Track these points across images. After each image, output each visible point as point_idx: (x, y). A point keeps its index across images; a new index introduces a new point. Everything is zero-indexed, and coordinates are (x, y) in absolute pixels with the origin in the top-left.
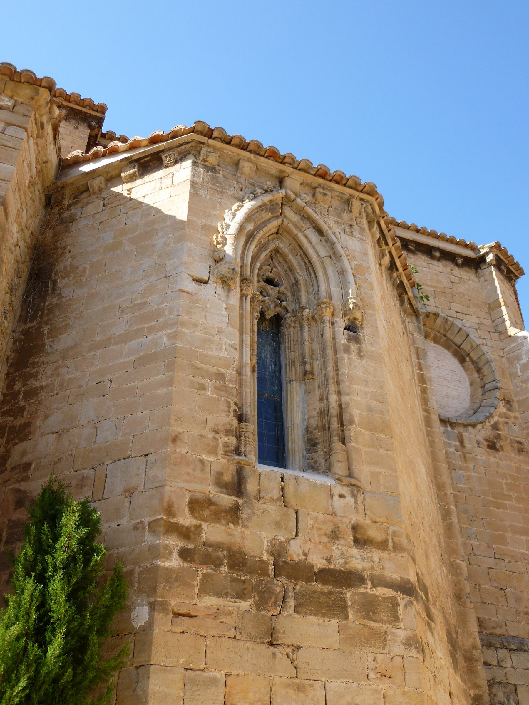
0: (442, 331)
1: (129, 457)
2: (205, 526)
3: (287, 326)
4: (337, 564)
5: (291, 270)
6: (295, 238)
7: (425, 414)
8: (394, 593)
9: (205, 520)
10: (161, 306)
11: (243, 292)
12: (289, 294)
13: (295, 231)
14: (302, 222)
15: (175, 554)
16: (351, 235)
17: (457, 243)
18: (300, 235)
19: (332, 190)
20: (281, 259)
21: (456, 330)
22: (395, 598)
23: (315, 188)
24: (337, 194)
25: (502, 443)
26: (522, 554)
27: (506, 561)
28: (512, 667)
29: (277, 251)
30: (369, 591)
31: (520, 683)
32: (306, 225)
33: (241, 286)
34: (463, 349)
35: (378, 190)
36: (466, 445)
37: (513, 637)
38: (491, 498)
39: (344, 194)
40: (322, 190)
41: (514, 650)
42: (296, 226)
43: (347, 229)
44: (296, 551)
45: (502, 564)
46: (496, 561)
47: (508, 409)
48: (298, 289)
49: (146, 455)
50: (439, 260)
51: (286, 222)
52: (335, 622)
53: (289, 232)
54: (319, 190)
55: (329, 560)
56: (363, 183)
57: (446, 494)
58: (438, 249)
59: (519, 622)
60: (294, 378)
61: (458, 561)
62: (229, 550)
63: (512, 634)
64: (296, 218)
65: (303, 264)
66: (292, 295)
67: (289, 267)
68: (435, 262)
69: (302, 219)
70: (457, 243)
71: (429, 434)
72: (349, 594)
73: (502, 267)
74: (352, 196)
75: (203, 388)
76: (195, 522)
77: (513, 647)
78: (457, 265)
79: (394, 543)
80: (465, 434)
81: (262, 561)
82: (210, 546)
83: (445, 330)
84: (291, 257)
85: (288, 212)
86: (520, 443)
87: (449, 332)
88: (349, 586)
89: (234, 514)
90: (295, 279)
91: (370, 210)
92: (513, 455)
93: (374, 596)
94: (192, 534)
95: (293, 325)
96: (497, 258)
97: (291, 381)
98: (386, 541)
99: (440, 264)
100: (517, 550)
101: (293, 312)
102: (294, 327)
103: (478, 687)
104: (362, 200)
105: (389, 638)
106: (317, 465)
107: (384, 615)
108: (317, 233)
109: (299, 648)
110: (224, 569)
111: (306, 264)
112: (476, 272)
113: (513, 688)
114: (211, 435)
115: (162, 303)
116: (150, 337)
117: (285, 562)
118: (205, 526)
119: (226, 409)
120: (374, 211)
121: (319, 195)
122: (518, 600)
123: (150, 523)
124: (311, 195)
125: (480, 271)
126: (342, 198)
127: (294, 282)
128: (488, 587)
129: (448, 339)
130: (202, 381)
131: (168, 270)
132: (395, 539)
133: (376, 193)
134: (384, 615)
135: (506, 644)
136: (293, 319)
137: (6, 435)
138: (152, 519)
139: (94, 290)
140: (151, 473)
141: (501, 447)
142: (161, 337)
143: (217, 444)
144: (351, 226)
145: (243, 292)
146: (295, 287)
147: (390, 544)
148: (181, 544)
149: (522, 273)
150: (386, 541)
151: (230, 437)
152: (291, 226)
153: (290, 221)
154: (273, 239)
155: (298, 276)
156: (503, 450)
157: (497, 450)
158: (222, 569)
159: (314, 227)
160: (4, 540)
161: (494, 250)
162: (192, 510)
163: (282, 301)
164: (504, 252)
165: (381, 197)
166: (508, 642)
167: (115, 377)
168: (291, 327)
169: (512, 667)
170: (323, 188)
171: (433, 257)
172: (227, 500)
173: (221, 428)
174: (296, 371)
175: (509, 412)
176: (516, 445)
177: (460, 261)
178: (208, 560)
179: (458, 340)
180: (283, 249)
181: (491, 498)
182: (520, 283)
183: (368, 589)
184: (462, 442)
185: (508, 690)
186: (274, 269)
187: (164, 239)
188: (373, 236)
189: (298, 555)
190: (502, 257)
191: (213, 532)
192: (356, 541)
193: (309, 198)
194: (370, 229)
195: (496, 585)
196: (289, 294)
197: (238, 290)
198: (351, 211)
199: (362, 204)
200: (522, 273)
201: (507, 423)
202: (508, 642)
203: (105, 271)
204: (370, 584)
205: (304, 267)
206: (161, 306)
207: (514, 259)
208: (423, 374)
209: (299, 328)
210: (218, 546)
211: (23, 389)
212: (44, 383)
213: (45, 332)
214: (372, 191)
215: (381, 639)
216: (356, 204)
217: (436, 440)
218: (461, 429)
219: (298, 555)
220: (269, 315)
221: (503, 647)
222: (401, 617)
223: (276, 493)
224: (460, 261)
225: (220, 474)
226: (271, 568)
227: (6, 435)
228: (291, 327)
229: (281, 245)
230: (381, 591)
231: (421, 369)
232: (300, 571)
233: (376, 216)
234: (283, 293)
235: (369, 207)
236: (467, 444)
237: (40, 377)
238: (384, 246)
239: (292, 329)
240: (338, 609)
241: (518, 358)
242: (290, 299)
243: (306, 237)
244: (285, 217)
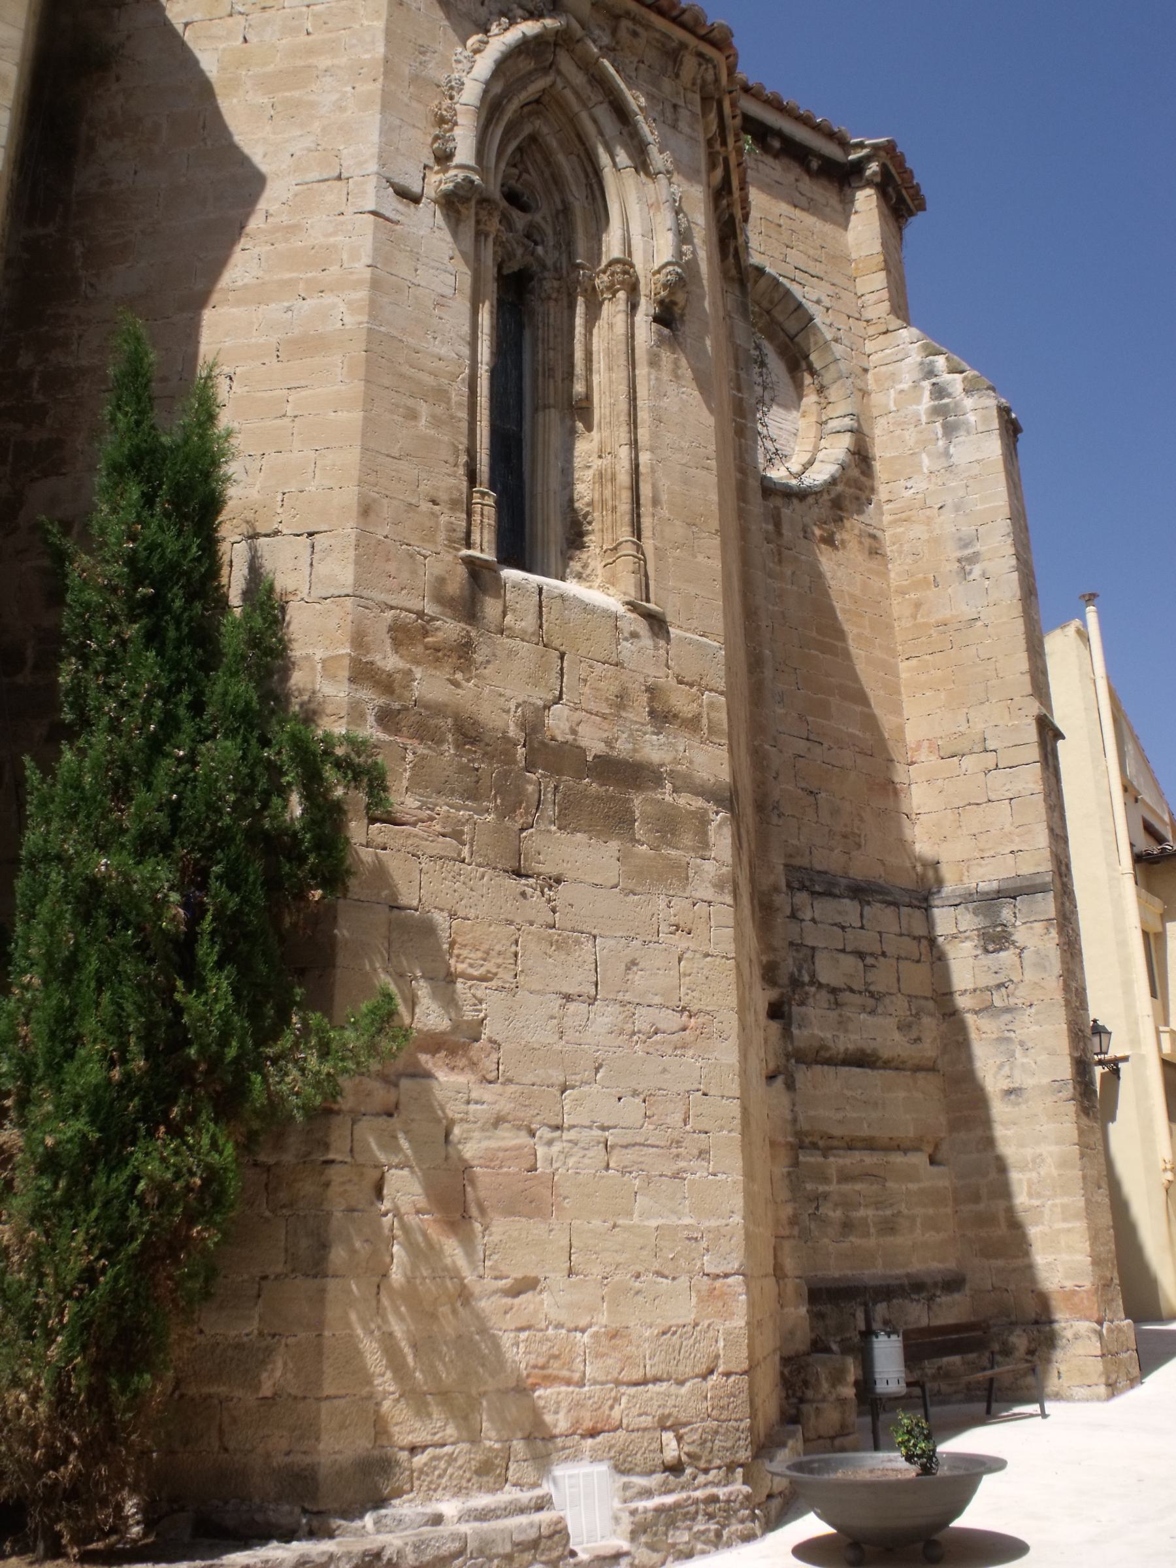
0: (765, 304)
1: (276, 533)
2: (418, 672)
3: (543, 295)
4: (623, 748)
5: (556, 182)
6: (573, 120)
7: (739, 476)
8: (706, 805)
9: (418, 663)
10: (332, 240)
11: (482, 227)
12: (549, 231)
13: (576, 106)
14: (589, 88)
15: (371, 719)
16: (674, 127)
17: (816, 128)
18: (584, 116)
19: (648, 26)
20: (538, 157)
21: (792, 307)
22: (706, 811)
23: (617, 18)
24: (658, 36)
25: (846, 536)
26: (851, 736)
27: (826, 746)
28: (813, 920)
29: (533, 138)
30: (668, 798)
31: (821, 945)
32: (595, 97)
33: (477, 214)
34: (798, 345)
35: (735, 41)
36: (784, 531)
37: (819, 872)
38: (814, 634)
39: (669, 37)
40: (630, 24)
41: (820, 894)
42: (577, 93)
43: (669, 113)
44: (558, 722)
45: (818, 750)
46: (809, 744)
47: (863, 473)
48: (570, 224)
49: (311, 534)
50: (776, 156)
51: (560, 85)
52: (614, 845)
53: (562, 105)
54: (625, 24)
55: (609, 743)
56: (709, 23)
57: (758, 628)
58: (779, 134)
59: (832, 850)
60: (552, 401)
61: (767, 747)
62: (457, 718)
63: (818, 867)
64: (579, 79)
65: (582, 176)
66: (555, 233)
67: (553, 175)
68: (769, 160)
69: (589, 82)
70: (816, 128)
71: (742, 514)
72: (638, 802)
73: (890, 190)
74: (683, 46)
75: (413, 415)
76: (402, 665)
77: (817, 888)
78: (808, 171)
79: (710, 721)
80: (786, 512)
81: (505, 738)
82: (426, 707)
83: (771, 302)
84: (561, 158)
85: (566, 63)
86: (874, 537)
87: (779, 308)
88: (639, 788)
89: (463, 654)
90: (563, 201)
91: (710, 77)
92: (860, 558)
93: (673, 807)
94: (396, 685)
95: (554, 295)
96: (885, 171)
97: (546, 407)
98: (697, 718)
99: (776, 164)
100: (844, 728)
101: (556, 269)
102: (556, 300)
103: (774, 950)
104: (700, 55)
105: (691, 873)
106: (588, 571)
107: (688, 839)
108: (614, 116)
109: (558, 881)
110: (449, 749)
111: (587, 176)
112: (841, 190)
113: (809, 952)
114: (425, 506)
115: (334, 234)
116: (309, 301)
117: (543, 743)
118: (418, 672)
119: (451, 460)
120: (717, 80)
121: (623, 34)
122: (835, 812)
123: (323, 661)
124: (608, 31)
125: (848, 191)
126: (663, 45)
127: (560, 207)
128: (790, 787)
129: (773, 321)
130: (410, 402)
131: (345, 164)
132: (712, 714)
133: (730, 46)
134: (688, 839)
135: (807, 883)
136: (556, 284)
137: (10, 458)
138: (330, 653)
139: (183, 180)
140: (321, 569)
141: (843, 542)
142: (334, 306)
143: (437, 523)
144: (675, 106)
145: (482, 227)
146: (561, 217)
147: (705, 721)
148: (381, 701)
149: (922, 207)
150: (697, 718)
151: (458, 515)
152: (569, 94)
153: (568, 83)
154: (530, 114)
155: (571, 199)
156: (844, 548)
157: (836, 548)
158: (445, 747)
159: (611, 103)
160: (30, 663)
161: (882, 153)
162: (397, 644)
163: (536, 244)
164: (899, 160)
165: (736, 55)
166: (811, 880)
167: (238, 370)
168: (549, 298)
169: (813, 920)
170: (634, 19)
171: (766, 149)
172: (450, 629)
173: (443, 496)
174: (556, 388)
175: (863, 479)
176: (867, 541)
177: (815, 164)
178: (423, 733)
179: (792, 326)
180: (548, 138)
181: (814, 634)
182: (916, 223)
183: (666, 794)
184: (778, 525)
185: (801, 956)
186: (525, 176)
187: (335, 97)
188: (706, 129)
189: (563, 733)
190: (893, 171)
191: (430, 685)
192: (651, 713)
193: (606, 40)
194: (705, 114)
195: (803, 785)
196: (549, 231)
197: (473, 222)
198: (677, 76)
199: (700, 65)
200: (922, 207)
201: (858, 499)
202: (811, 880)
203: (204, 140)
204: (669, 786)
205: (584, 181)
206: (332, 240)
207: (912, 177)
208: (741, 399)
209: (565, 304)
210: (438, 710)
211: (40, 368)
212: (84, 363)
213: (78, 252)
214: (720, 41)
215: (680, 874)
216: (689, 64)
217: (753, 527)
218: (779, 501)
219: (563, 733)
220: (513, 267)
221: (803, 887)
222: (712, 840)
223: (528, 623)
224: (815, 164)
225: (441, 581)
226: (521, 750)
227: (10, 458)
228: (549, 298)
229: (545, 130)
230: (686, 801)
231: (739, 390)
232: (548, 754)
233: (718, 89)
234: (538, 228)
235: (711, 71)
236: (786, 530)
237: (74, 347)
238: (718, 147)
239: (552, 303)
240: (617, 822)
241: (893, 378)
242: (551, 242)
243: (595, 121)
244: (559, 72)
